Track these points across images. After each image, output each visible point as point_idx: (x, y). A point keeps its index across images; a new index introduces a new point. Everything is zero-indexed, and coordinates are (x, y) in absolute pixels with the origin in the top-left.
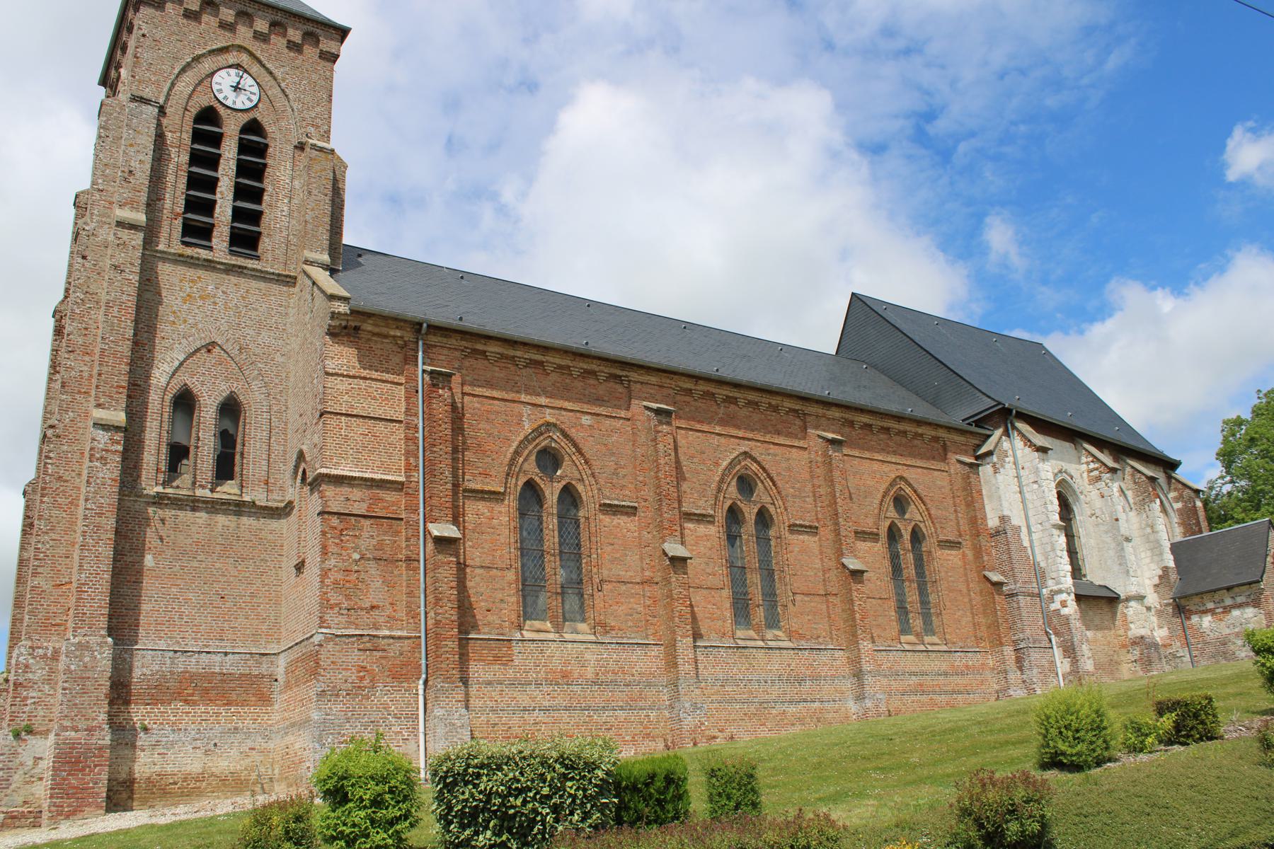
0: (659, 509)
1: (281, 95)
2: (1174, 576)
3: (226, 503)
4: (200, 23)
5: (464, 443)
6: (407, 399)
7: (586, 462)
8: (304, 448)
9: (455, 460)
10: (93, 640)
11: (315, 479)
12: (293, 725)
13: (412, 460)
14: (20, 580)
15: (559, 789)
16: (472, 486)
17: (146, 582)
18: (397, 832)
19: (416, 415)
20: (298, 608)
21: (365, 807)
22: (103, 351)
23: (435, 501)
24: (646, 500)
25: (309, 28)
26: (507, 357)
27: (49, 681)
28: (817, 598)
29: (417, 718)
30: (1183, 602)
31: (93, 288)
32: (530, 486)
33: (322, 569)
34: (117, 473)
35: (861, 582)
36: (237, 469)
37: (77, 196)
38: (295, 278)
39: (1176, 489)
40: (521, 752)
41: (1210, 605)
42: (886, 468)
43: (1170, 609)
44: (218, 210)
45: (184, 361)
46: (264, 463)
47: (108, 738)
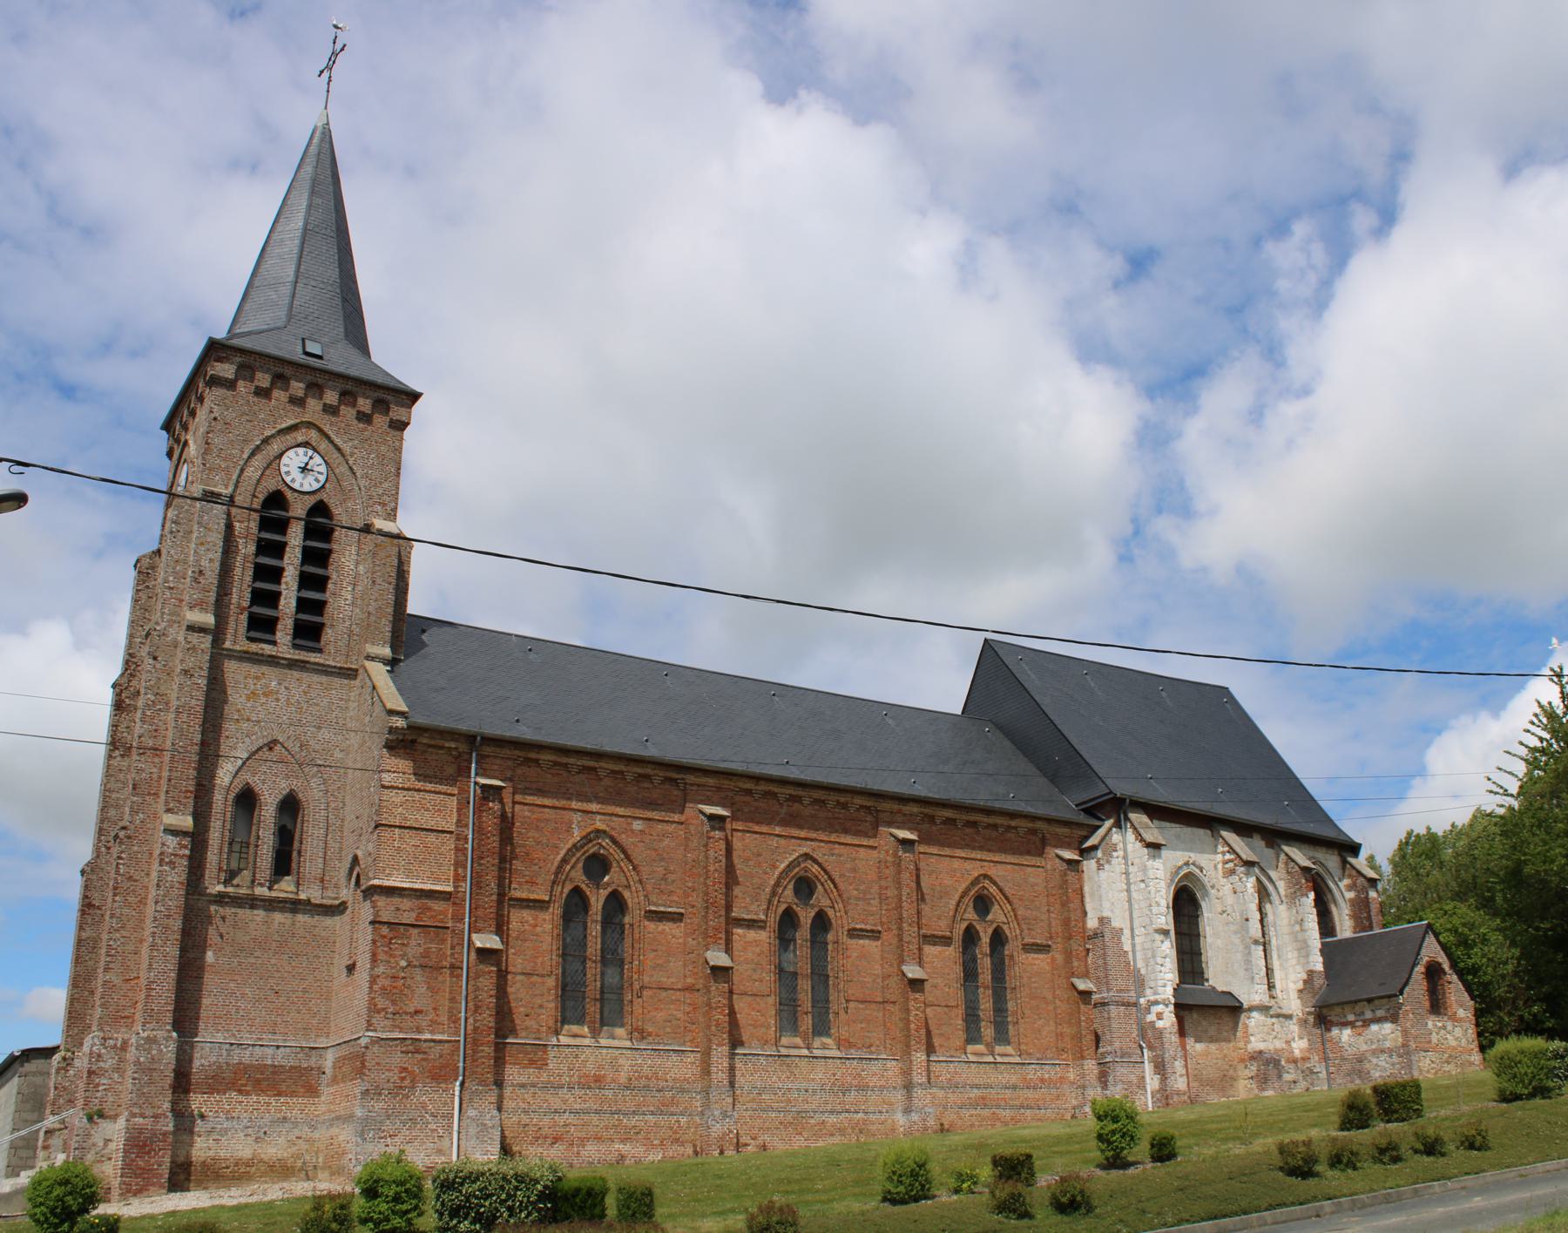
0: (705, 917)
1: (348, 473)
2: (1319, 982)
3: (285, 901)
5: (512, 852)
6: (459, 810)
7: (635, 868)
8: (359, 853)
9: (501, 869)
10: (160, 1034)
16: (518, 894)
17: (208, 978)
19: (467, 826)
20: (348, 1010)
25: (380, 394)
26: (560, 764)
27: (118, 1070)
28: (873, 1006)
30: (1325, 1011)
31: (163, 689)
32: (577, 891)
34: (184, 876)
35: (922, 991)
36: (294, 865)
39: (1350, 876)
41: (1351, 1018)
42: (968, 865)
43: (1311, 1019)
44: (282, 602)
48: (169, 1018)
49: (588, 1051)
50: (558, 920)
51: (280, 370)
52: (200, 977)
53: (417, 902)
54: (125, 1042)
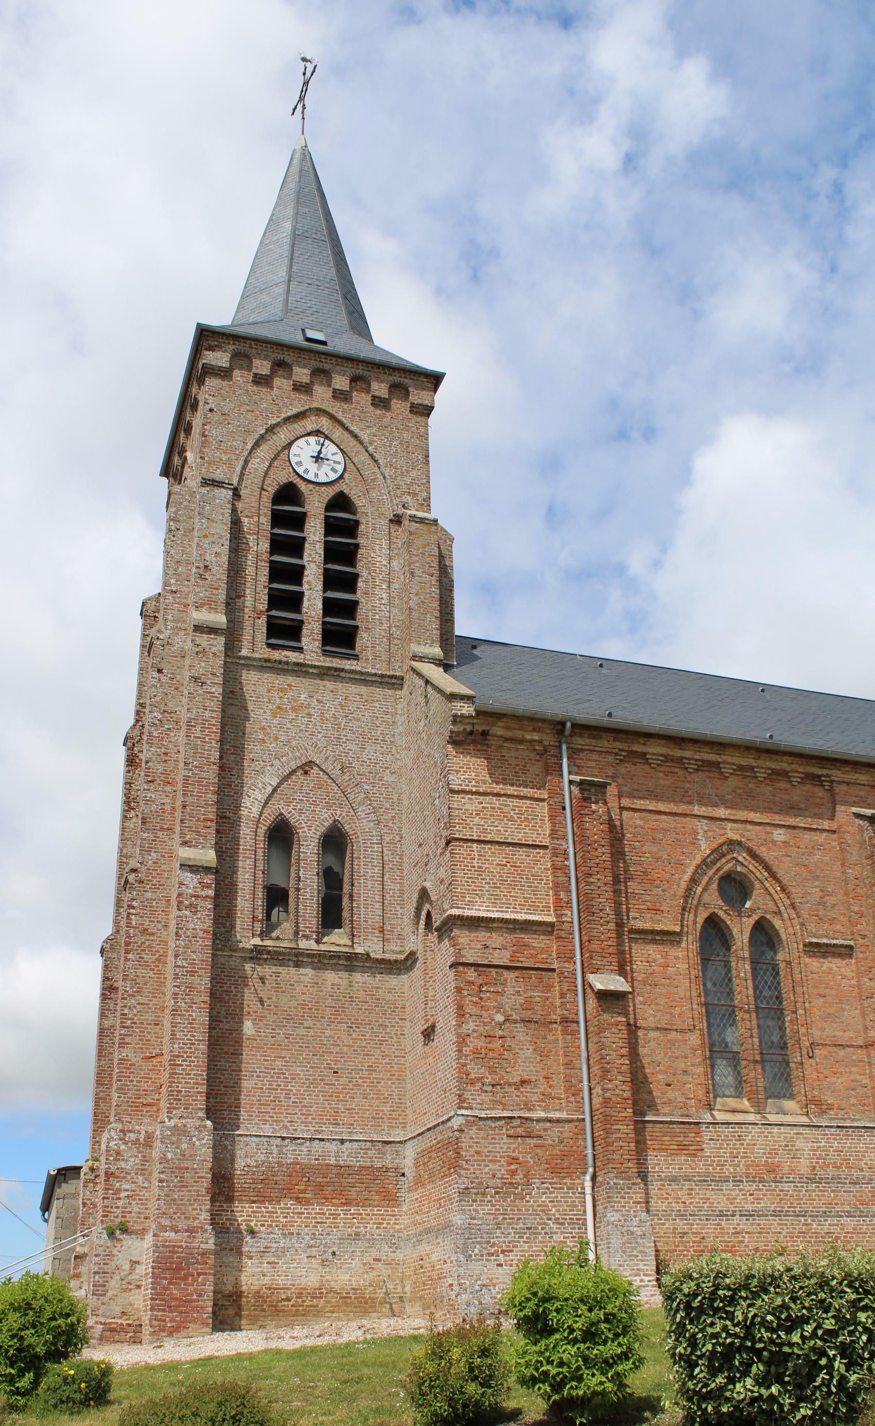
1: (369, 461)
4: (272, 388)
5: (626, 871)
6: (552, 818)
7: (783, 889)
8: (428, 885)
9: (617, 892)
10: (191, 1123)
11: (445, 923)
12: (428, 1231)
13: (562, 895)
14: (102, 1052)
15: (848, 1323)
16: (640, 924)
18: (618, 1374)
19: (564, 837)
20: (427, 1086)
21: (575, 1341)
22: (186, 778)
23: (594, 946)
24: (864, 937)
25: (396, 378)
26: (673, 759)
27: (142, 1171)
29: (585, 1224)
31: (171, 706)
32: (712, 921)
33: (459, 1035)
34: (208, 923)
36: (346, 914)
37: (144, 604)
38: (402, 678)
40: (789, 1270)
44: (306, 604)
45: (278, 786)
46: (378, 905)
47: (212, 1241)
48: (201, 1102)
49: (757, 1129)
50: (696, 960)
51: (279, 357)
52: (238, 1054)
53: (510, 937)
54: (149, 1137)
